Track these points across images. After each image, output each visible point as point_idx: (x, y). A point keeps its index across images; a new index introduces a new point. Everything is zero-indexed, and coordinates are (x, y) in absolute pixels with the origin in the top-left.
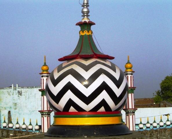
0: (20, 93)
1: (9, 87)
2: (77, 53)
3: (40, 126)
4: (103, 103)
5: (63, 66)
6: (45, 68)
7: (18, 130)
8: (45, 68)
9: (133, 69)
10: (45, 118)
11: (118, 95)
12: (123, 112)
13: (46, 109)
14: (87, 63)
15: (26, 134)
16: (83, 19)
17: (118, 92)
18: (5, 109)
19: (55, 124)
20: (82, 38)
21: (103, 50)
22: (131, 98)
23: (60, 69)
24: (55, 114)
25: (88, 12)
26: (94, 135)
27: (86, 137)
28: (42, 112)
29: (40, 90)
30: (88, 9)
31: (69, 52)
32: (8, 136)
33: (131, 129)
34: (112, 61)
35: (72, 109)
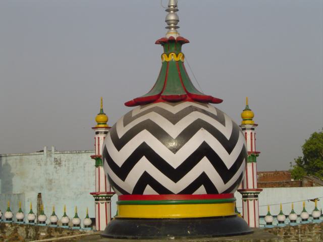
0: (58, 162)
2: (157, 93)
3: (93, 220)
4: (203, 179)
5: (134, 115)
6: (102, 118)
7: (55, 226)
8: (102, 118)
9: (255, 121)
10: (102, 206)
12: (238, 196)
13: (103, 190)
14: (175, 109)
15: (68, 233)
16: (168, 33)
17: (229, 160)
18: (32, 189)
19: (119, 216)
20: (166, 65)
21: (202, 87)
22: (250, 173)
23: (127, 119)
24: (120, 198)
28: (96, 196)
29: (93, 157)
31: (144, 91)
33: (252, 225)
35: (149, 190)
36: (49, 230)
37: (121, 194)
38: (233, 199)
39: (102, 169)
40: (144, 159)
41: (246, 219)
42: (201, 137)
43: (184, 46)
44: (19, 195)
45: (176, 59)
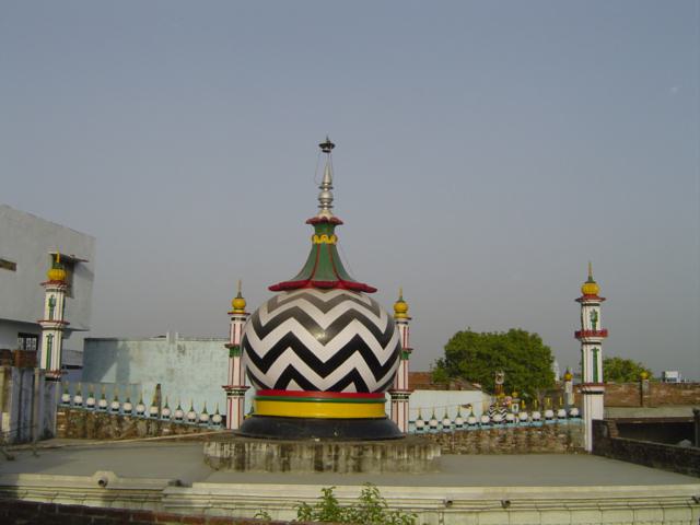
0: (182, 350)
1: (101, 344)
2: (305, 278)
3: (224, 417)
4: (354, 376)
5: (280, 300)
6: (239, 302)
7: (180, 422)
8: (239, 302)
9: (409, 314)
10: (235, 402)
11: (382, 363)
12: (388, 396)
13: (236, 383)
14: (326, 297)
15: (195, 431)
16: (321, 212)
17: (383, 356)
18: (151, 379)
19: (256, 413)
20: (317, 247)
21: (355, 274)
22: (402, 370)
23: (272, 305)
24: (258, 393)
25: (331, 200)
26: (333, 437)
27: (318, 440)
28: (229, 390)
29: (227, 346)
30: (331, 194)
31: (290, 276)
32: (159, 433)
33: (401, 429)
34: (371, 295)
35: (293, 386)
36: (174, 426)
37: (260, 388)
38: (381, 399)
39: (237, 360)
40: (289, 350)
41: (394, 420)
42: (354, 329)
43: (337, 227)
44: (135, 385)
45: (330, 242)
